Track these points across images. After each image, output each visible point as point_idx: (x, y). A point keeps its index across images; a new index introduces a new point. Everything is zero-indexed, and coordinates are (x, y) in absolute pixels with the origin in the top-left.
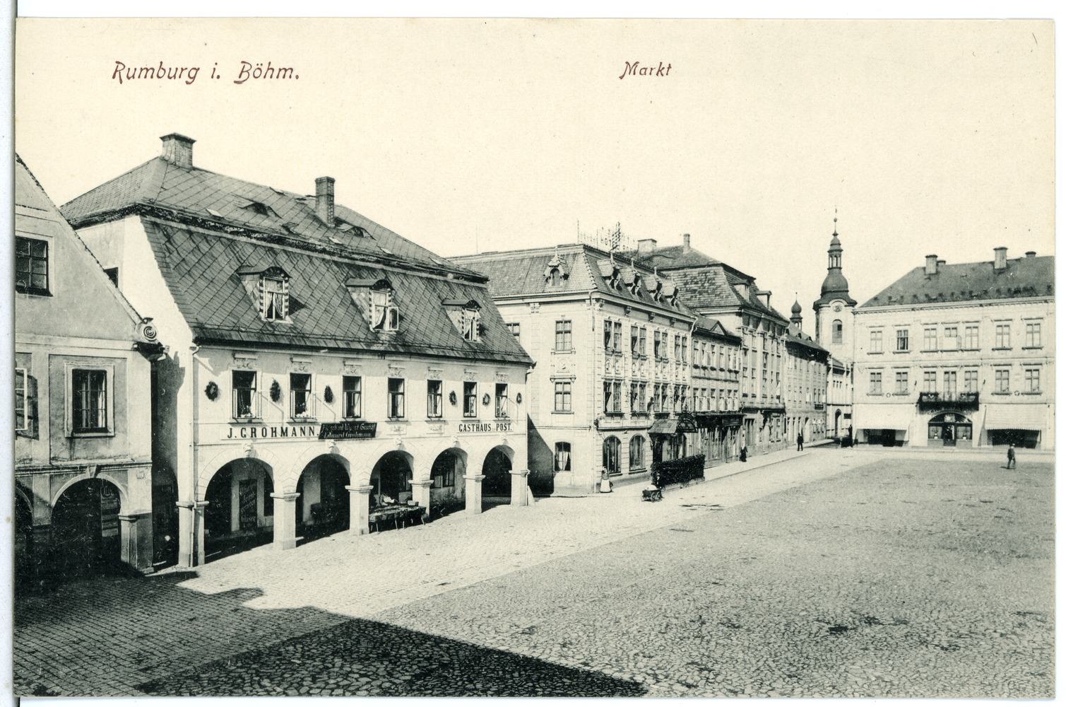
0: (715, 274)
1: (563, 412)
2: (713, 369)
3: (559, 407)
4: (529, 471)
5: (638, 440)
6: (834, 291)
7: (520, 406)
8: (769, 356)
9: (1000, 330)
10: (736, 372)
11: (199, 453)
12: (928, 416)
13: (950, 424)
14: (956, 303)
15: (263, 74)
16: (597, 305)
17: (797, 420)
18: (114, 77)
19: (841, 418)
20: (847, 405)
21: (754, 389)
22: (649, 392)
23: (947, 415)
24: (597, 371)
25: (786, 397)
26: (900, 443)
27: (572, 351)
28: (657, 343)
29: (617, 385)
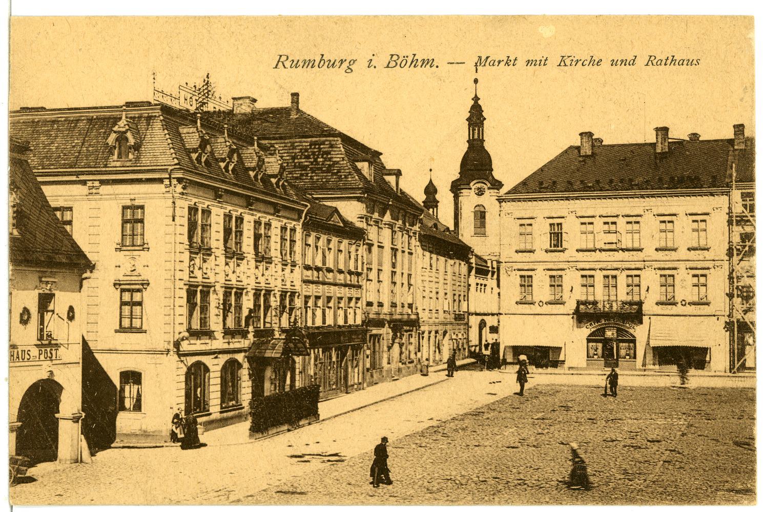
0: (332, 146)
1: (131, 329)
2: (329, 270)
3: (126, 323)
4: (84, 414)
5: (231, 368)
6: (476, 166)
7: (72, 324)
8: (399, 254)
9: (663, 226)
10: (359, 274)
12: (586, 331)
13: (611, 340)
14: (616, 193)
16: (179, 188)
17: (433, 333)
19: (486, 331)
20: (493, 315)
21: (378, 293)
22: (248, 303)
23: (610, 327)
24: (179, 275)
25: (420, 305)
26: (556, 364)
27: (144, 247)
28: (257, 237)
29: (205, 294)
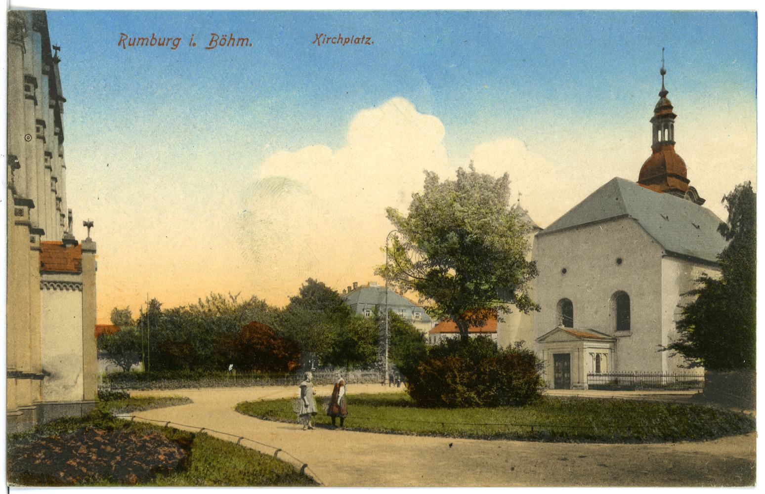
11: (87, 399)
15: (227, 43)
18: (119, 44)
